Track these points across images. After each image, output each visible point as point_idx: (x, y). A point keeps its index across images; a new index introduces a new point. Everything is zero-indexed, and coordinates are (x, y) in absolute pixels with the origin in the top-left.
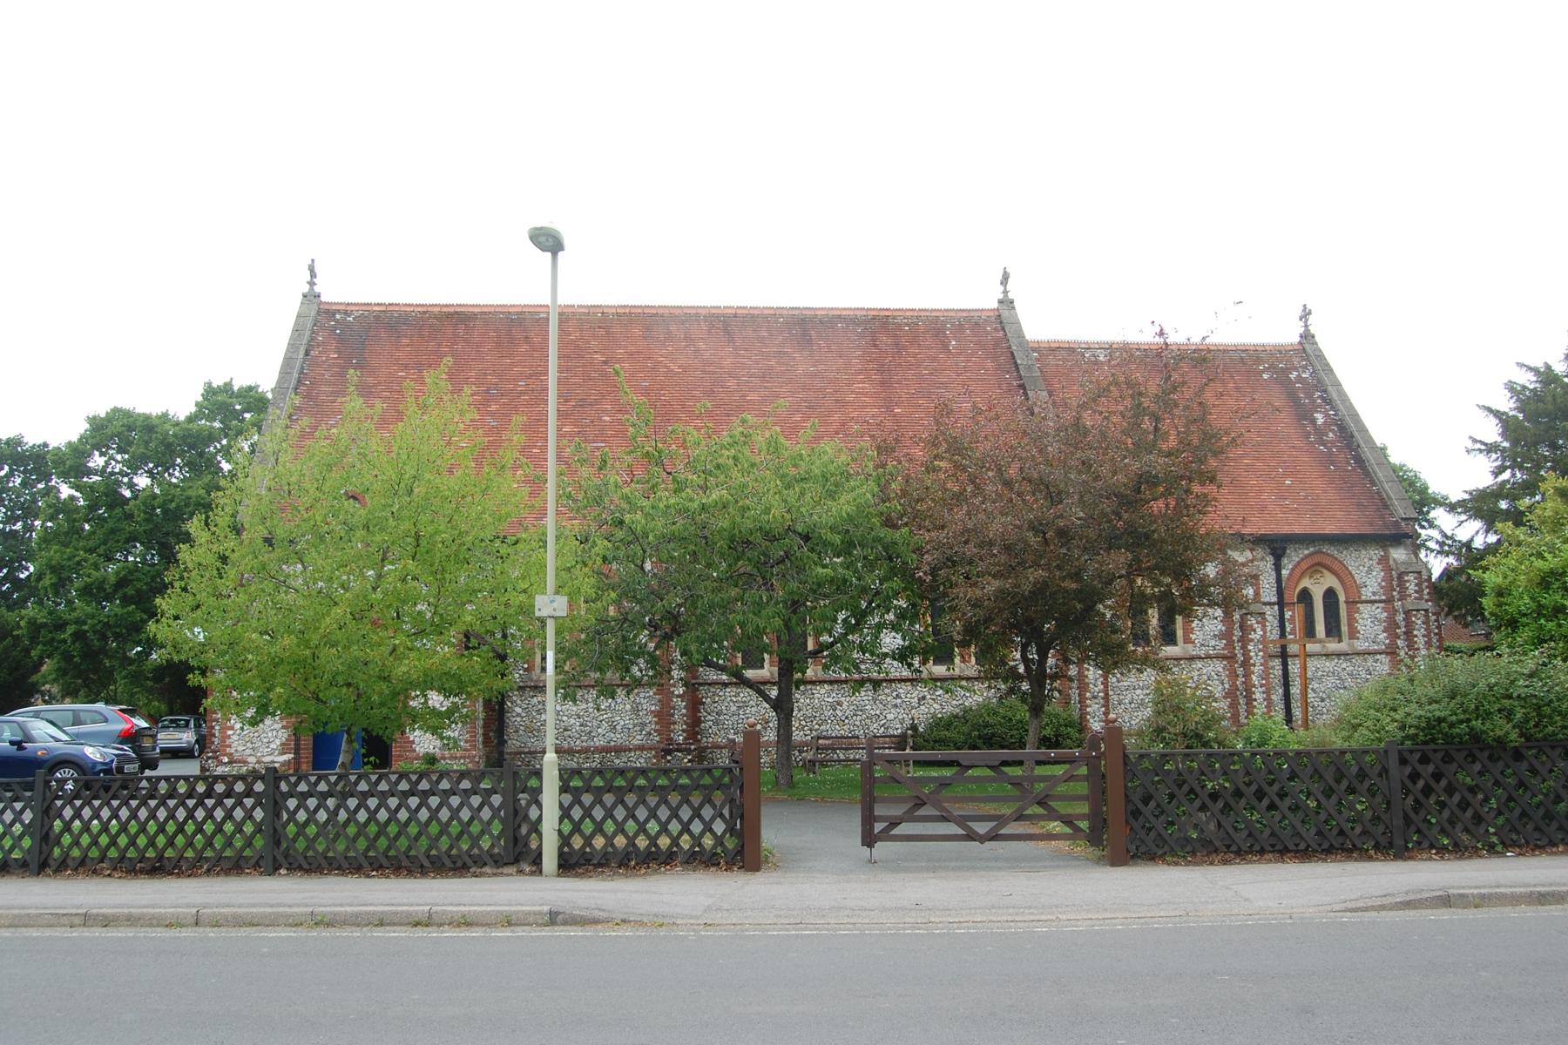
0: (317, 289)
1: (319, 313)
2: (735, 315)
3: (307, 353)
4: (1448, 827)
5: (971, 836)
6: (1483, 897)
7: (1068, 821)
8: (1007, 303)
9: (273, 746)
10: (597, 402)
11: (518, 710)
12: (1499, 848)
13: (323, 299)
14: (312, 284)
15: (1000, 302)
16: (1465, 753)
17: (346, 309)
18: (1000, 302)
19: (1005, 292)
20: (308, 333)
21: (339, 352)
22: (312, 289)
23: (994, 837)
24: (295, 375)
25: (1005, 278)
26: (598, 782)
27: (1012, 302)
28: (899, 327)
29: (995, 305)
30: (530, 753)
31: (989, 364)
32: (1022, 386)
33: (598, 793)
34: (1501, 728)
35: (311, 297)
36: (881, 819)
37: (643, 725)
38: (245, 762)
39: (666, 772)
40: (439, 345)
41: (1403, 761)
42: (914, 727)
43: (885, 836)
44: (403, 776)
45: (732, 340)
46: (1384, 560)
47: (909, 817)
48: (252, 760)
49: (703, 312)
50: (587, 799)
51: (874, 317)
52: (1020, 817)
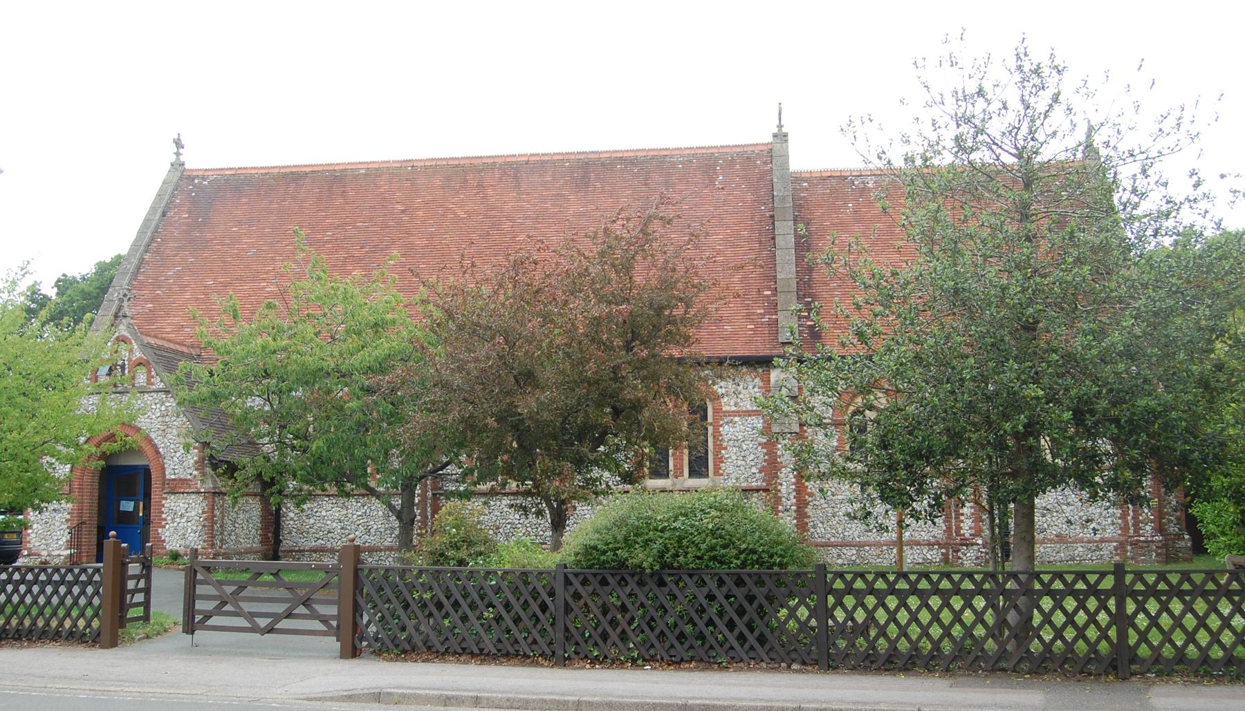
0: (182, 158)
1: (181, 178)
2: (527, 163)
3: (164, 214)
4: (600, 641)
5: (254, 629)
6: (404, 696)
7: (324, 620)
8: (781, 137)
10: (387, 247)
11: (291, 515)
12: (640, 662)
13: (187, 166)
14: (178, 154)
15: (775, 136)
16: (618, 578)
17: (204, 175)
18: (775, 136)
19: (780, 126)
20: (167, 197)
21: (189, 213)
22: (178, 158)
23: (270, 630)
24: (149, 234)
27: (786, 135)
28: (674, 164)
29: (770, 139)
30: (299, 551)
31: (749, 197)
32: (772, 217)
33: (923, 596)
34: (642, 557)
35: (178, 165)
36: (200, 612)
39: (948, 575)
40: (271, 202)
41: (568, 582)
43: (202, 625)
44: (18, 569)
45: (518, 186)
47: (218, 611)
48: (44, 553)
49: (499, 161)
50: (913, 602)
51: (653, 158)
52: (289, 615)
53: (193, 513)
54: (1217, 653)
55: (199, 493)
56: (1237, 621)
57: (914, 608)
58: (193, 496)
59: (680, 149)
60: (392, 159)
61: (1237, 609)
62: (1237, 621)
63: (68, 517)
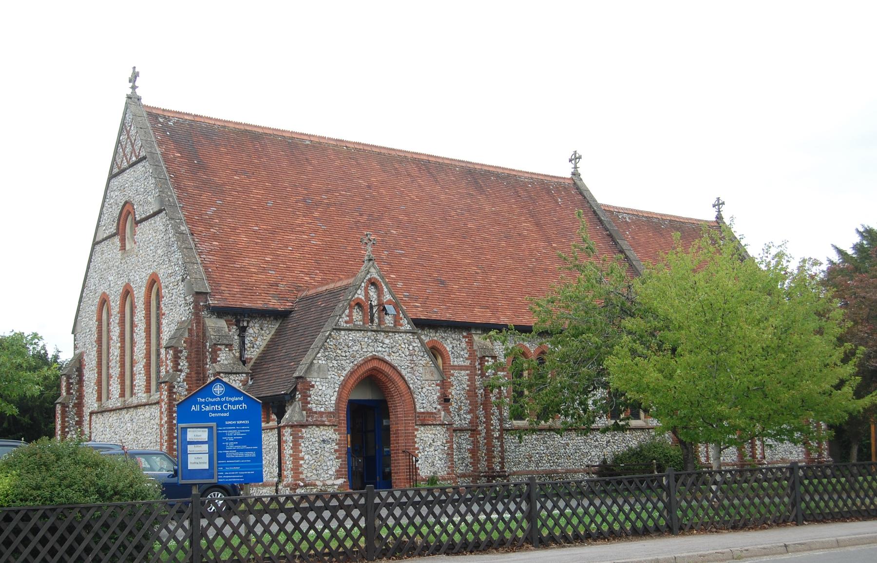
9: (331, 472)
14: (576, 168)
15: (129, 97)
25: (135, 76)
26: (319, 503)
29: (569, 176)
33: (319, 511)
35: (133, 99)
37: (463, 459)
38: (315, 485)
42: (604, 461)
46: (470, 343)
48: (318, 483)
50: (297, 516)
53: (439, 443)
54: (495, 536)
55: (442, 425)
56: (874, 484)
57: (341, 518)
58: (438, 428)
59: (201, 117)
60: (327, 135)
61: (874, 479)
62: (874, 484)
63: (337, 447)
